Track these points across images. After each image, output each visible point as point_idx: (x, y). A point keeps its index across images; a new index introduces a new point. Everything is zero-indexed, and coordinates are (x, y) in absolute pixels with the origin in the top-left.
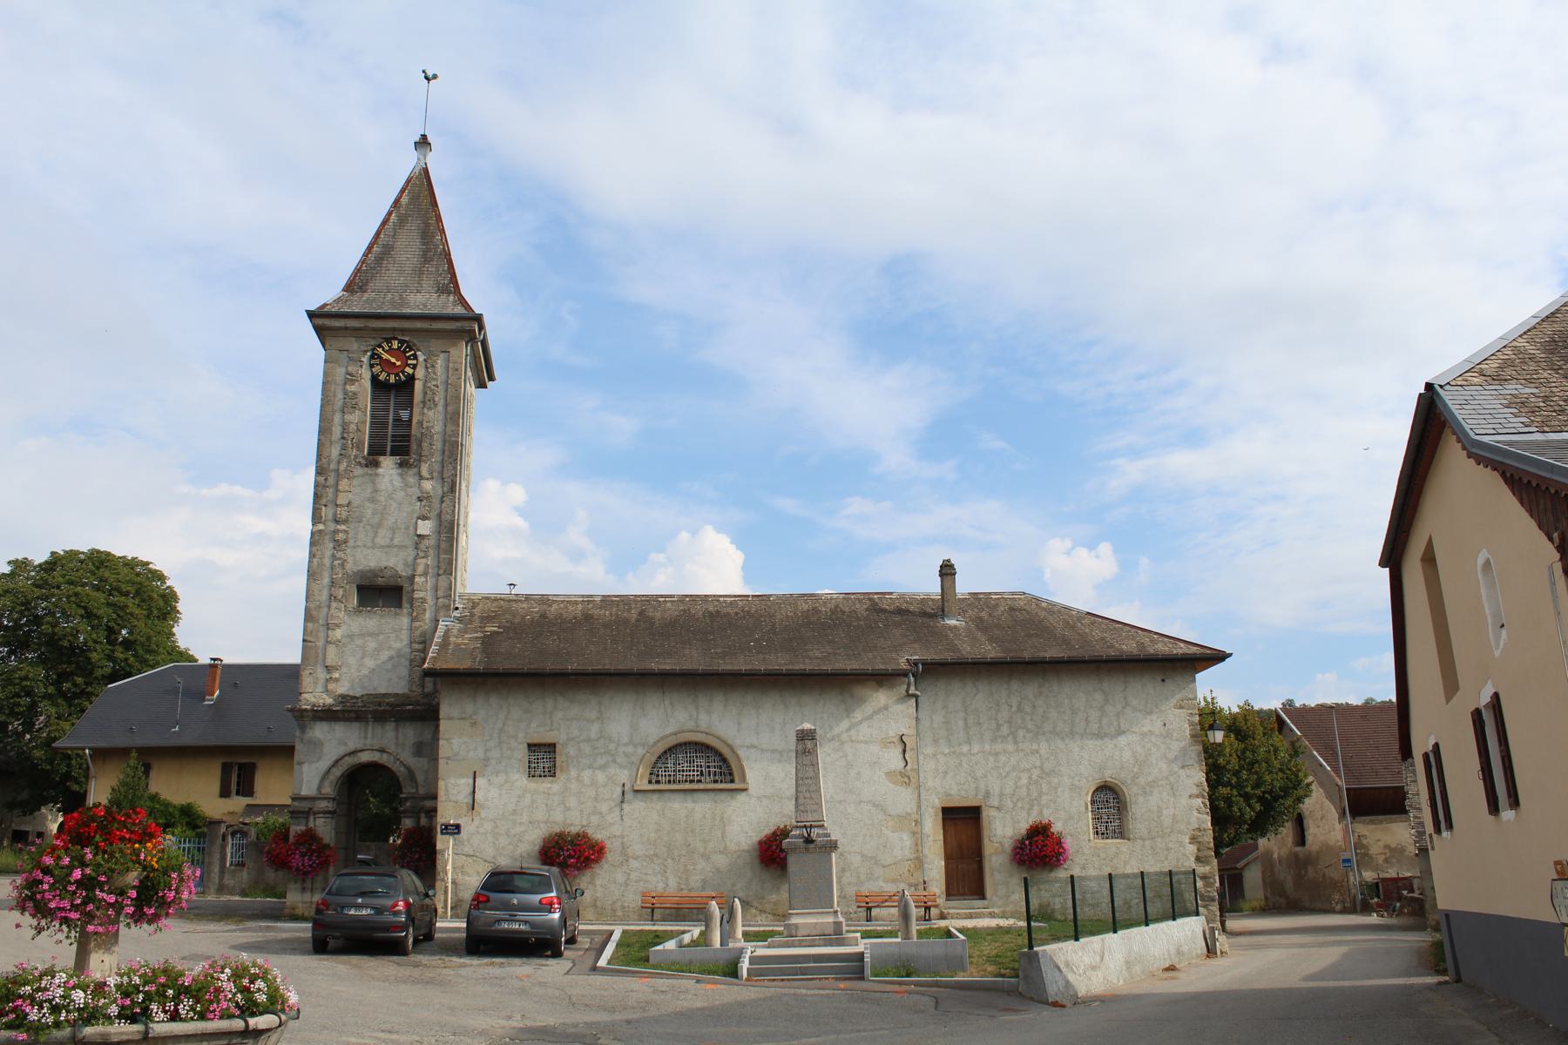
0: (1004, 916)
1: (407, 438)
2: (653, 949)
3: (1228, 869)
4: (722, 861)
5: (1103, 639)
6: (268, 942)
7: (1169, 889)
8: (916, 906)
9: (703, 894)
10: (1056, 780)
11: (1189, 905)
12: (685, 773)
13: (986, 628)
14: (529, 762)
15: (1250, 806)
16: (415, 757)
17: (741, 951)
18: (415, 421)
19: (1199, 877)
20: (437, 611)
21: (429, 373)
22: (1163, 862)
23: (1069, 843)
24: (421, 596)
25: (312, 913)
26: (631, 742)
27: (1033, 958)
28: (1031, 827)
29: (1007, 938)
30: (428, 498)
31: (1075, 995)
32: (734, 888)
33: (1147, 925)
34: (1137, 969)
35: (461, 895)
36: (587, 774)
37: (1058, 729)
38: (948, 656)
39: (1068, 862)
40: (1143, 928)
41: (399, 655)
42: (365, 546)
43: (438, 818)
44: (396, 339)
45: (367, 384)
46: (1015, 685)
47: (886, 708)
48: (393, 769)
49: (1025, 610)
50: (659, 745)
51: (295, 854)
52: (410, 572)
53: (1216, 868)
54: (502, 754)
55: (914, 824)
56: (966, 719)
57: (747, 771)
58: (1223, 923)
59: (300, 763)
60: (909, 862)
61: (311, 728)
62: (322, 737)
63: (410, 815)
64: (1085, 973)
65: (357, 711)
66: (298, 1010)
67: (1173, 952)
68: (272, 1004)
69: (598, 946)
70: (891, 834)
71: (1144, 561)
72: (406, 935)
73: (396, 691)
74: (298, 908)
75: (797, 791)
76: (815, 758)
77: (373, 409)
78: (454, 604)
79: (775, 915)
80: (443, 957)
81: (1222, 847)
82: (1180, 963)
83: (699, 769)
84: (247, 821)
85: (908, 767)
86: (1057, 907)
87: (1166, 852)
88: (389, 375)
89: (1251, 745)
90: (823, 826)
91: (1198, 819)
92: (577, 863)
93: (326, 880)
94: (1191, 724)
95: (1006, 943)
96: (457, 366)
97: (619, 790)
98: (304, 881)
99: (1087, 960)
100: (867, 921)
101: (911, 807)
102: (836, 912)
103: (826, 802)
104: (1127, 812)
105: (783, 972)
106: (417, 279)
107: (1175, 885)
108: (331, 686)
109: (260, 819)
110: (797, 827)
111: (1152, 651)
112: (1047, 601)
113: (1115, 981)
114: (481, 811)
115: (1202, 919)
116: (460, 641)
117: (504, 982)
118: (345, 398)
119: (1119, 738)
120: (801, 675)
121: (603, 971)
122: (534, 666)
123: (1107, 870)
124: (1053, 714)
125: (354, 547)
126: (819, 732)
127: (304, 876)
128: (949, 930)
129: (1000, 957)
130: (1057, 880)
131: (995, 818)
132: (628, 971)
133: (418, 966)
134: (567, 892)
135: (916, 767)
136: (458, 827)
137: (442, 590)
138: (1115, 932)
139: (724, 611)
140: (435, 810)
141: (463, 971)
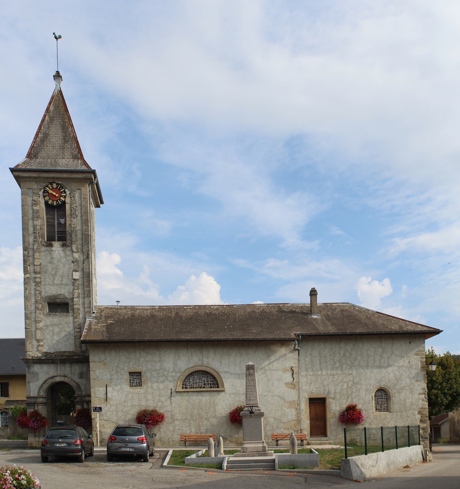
0: (335, 444)
1: (64, 232)
2: (186, 458)
3: (434, 425)
4: (214, 421)
5: (383, 324)
6: (22, 458)
7: (408, 434)
8: (297, 440)
9: (207, 435)
10: (359, 387)
11: (416, 440)
12: (198, 384)
13: (330, 319)
14: (130, 380)
15: (446, 398)
16: (79, 379)
17: (223, 459)
18: (67, 224)
19: (421, 428)
20: (85, 313)
21: (72, 200)
22: (405, 422)
23: (364, 413)
24: (77, 307)
25: (40, 445)
26: (174, 371)
27: (347, 462)
28: (348, 406)
29: (336, 453)
30: (77, 261)
31: (365, 477)
32: (220, 432)
33: (397, 448)
34: (392, 467)
35: (103, 437)
36: (155, 385)
37: (361, 364)
38: (313, 332)
39: (364, 422)
40: (395, 450)
41: (69, 334)
42: (50, 284)
43: (92, 405)
44: (55, 183)
45: (43, 206)
46: (342, 345)
47: (285, 355)
48: (71, 384)
49: (348, 311)
50: (187, 372)
51: (30, 421)
52: (71, 296)
53: (429, 425)
54: (118, 377)
55: (296, 405)
56: (320, 360)
57: (224, 383)
58: (430, 448)
59: (29, 383)
60: (295, 421)
61: (32, 367)
62: (37, 371)
63: (79, 403)
64: (369, 468)
65: (53, 359)
66: (40, 487)
67: (408, 460)
68: (29, 485)
69: (163, 457)
70: (287, 409)
71: (404, 288)
72: (82, 454)
73: (69, 350)
74: (33, 443)
75: (246, 391)
76: (254, 377)
77: (47, 218)
78: (92, 311)
79: (237, 443)
80: (98, 463)
81: (432, 416)
82: (410, 464)
83: (204, 382)
84: (7, 407)
85: (295, 381)
86: (358, 440)
87: (407, 418)
88: (53, 201)
89: (449, 371)
90: (257, 406)
91: (422, 403)
92: (152, 422)
93: (45, 432)
94: (421, 362)
95: (336, 455)
96: (85, 196)
97: (169, 391)
98: (35, 433)
99: (370, 463)
100: (277, 446)
101: (295, 398)
102: (263, 442)
103: (259, 396)
104: (391, 400)
105: (241, 467)
106: (62, 151)
107: (410, 432)
108: (40, 348)
109: (13, 407)
110: (247, 407)
111: (406, 329)
112: (358, 307)
113: (382, 472)
114: (110, 401)
115: (421, 446)
116: (96, 327)
117: (124, 473)
118: (33, 213)
119: (389, 368)
120: (248, 341)
121: (166, 467)
122: (130, 338)
123: (381, 425)
124: (359, 358)
125: (45, 285)
126: (256, 366)
127: (35, 431)
128: (311, 450)
129: (333, 461)
130: (359, 429)
131: (332, 402)
132: (176, 467)
133: (87, 467)
134: (149, 435)
135: (298, 381)
136: (100, 408)
137: (87, 304)
138: (383, 451)
139: (213, 312)
140: (90, 401)
141: (107, 469)
